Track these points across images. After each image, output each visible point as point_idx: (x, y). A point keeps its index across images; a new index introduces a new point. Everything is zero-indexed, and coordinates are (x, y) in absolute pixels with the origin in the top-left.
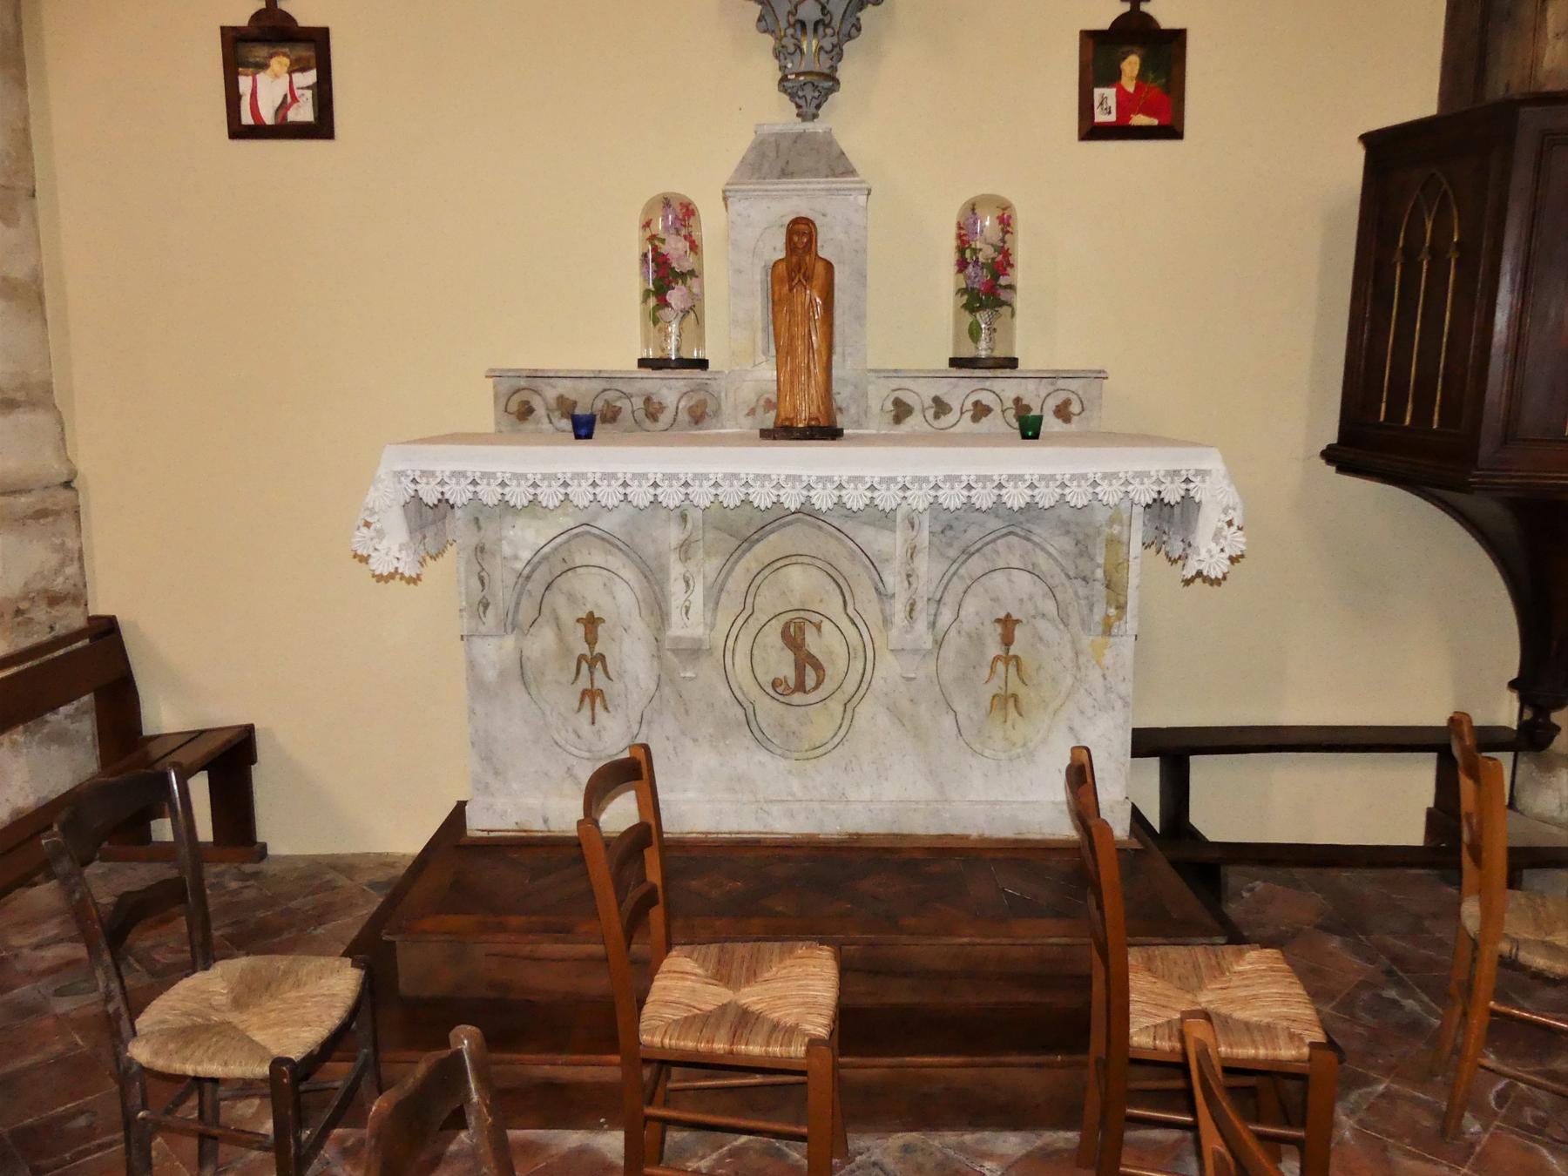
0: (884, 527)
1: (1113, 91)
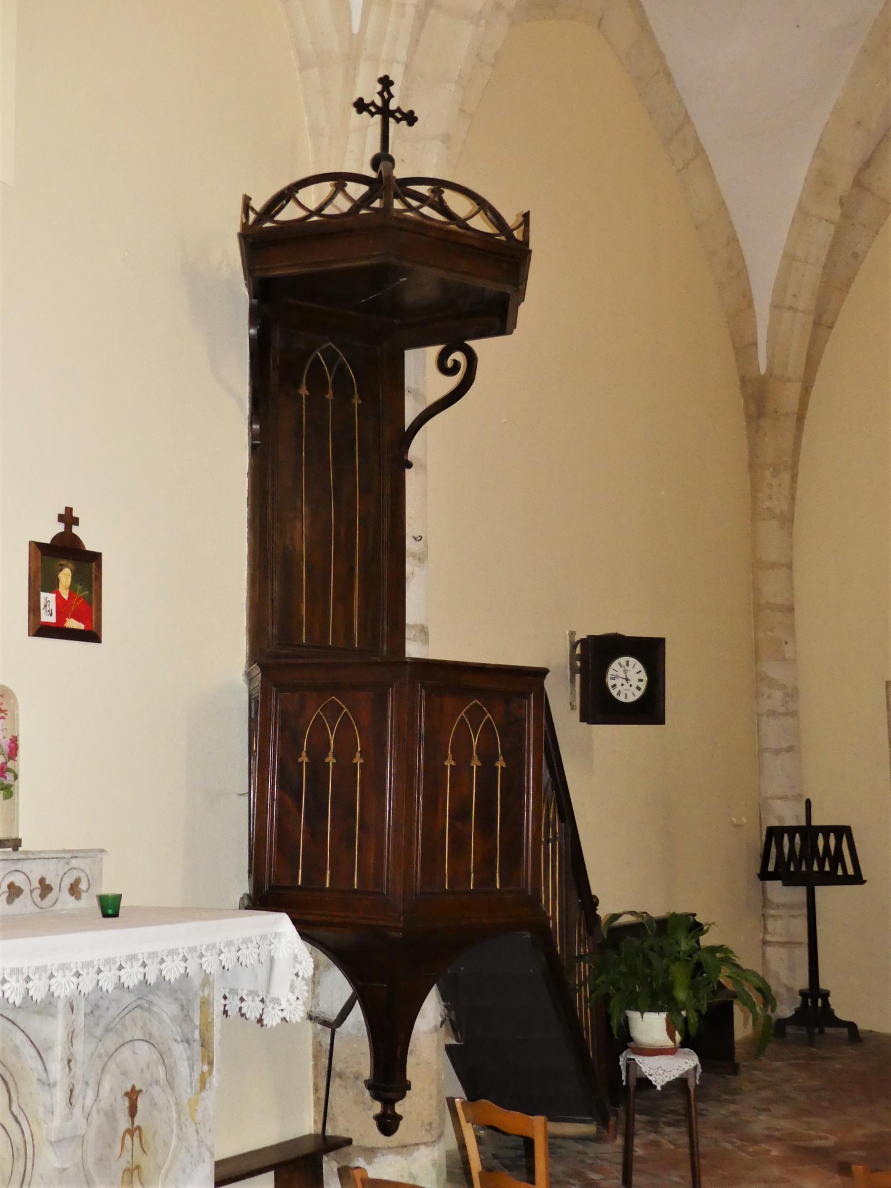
0: (48, 1014)
1: (54, 596)
